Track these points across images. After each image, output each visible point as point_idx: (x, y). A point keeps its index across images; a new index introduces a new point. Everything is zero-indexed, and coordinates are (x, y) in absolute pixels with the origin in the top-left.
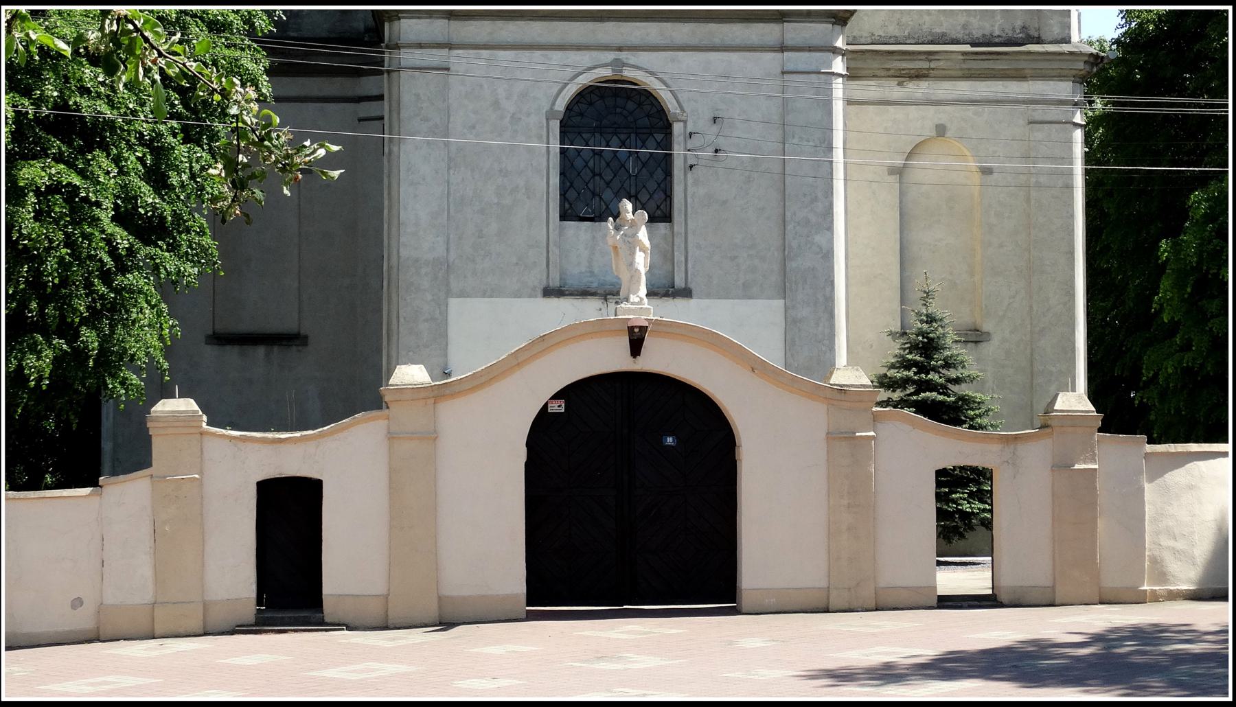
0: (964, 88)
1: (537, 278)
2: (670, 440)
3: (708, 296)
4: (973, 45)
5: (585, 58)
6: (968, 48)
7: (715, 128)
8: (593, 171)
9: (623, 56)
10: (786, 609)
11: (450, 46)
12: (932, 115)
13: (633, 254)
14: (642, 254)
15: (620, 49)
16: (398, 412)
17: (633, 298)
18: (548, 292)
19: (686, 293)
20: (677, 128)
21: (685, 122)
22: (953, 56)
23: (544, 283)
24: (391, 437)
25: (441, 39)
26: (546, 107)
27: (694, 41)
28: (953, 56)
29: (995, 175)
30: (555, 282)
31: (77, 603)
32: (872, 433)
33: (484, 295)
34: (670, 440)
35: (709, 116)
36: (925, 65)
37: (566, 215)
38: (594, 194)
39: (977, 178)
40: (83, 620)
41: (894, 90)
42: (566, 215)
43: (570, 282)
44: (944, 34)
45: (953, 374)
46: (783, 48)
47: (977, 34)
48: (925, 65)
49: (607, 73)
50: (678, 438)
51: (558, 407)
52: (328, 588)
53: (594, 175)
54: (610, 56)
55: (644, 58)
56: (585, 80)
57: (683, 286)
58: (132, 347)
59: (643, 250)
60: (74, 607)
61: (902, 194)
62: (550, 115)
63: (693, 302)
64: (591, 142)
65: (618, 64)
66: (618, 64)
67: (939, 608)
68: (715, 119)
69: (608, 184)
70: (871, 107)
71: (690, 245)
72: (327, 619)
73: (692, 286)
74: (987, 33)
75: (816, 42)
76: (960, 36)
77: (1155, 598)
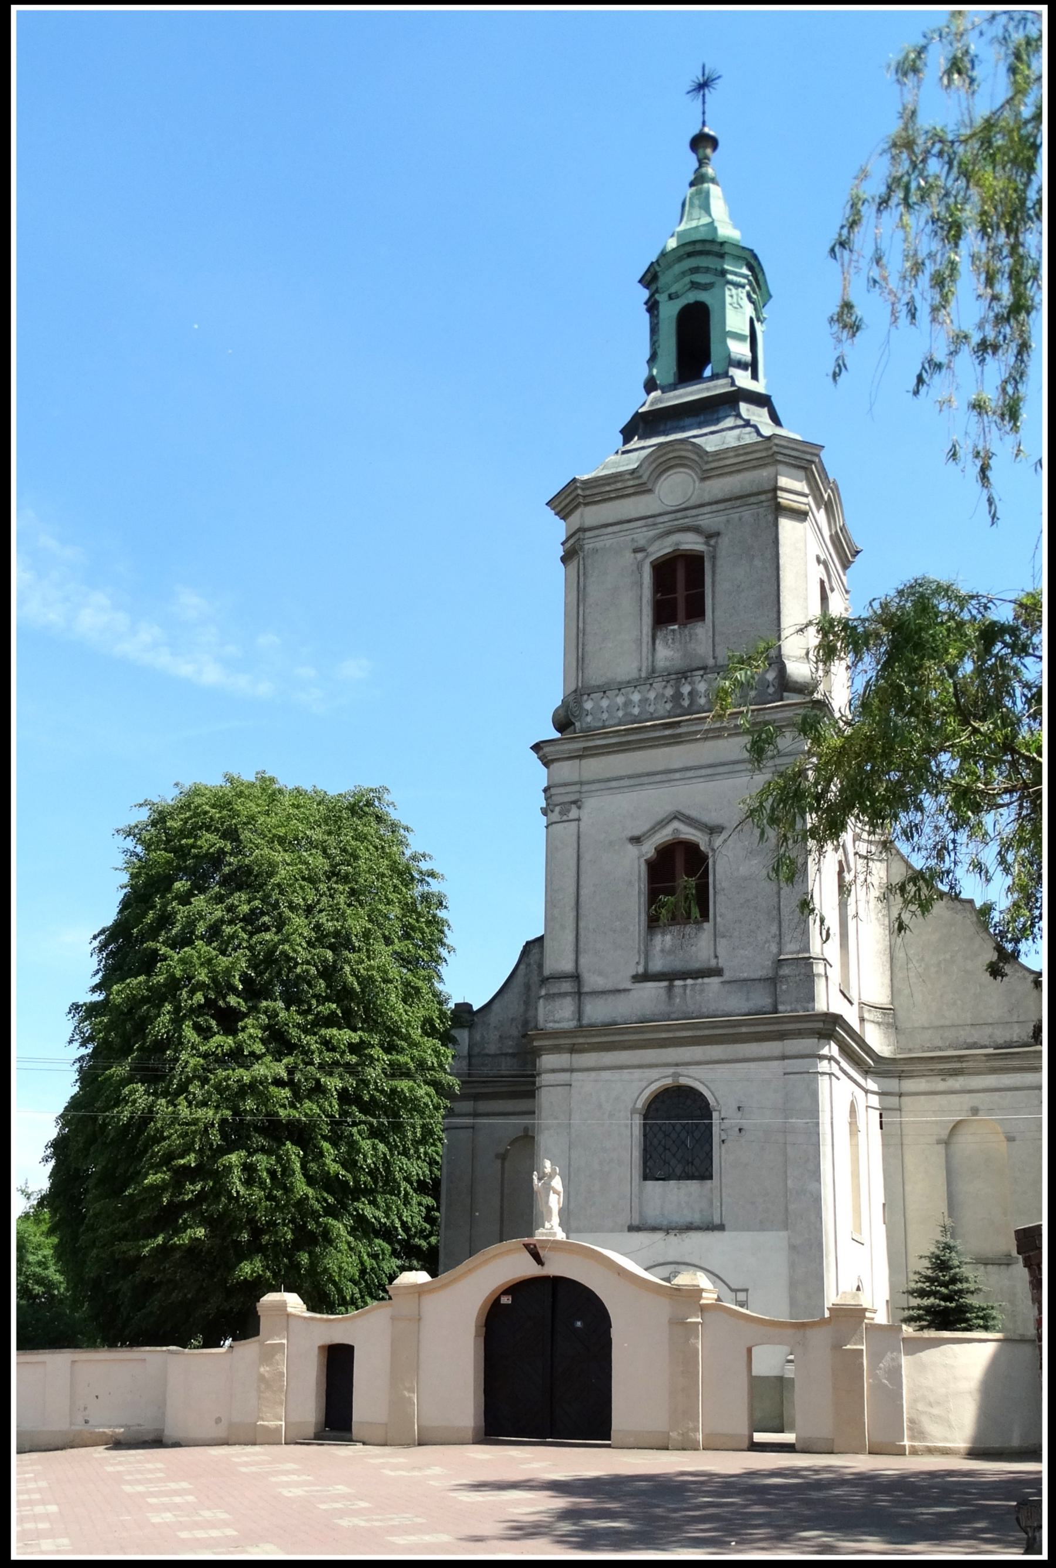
0: (991, 1081)
1: (624, 1220)
2: (579, 1324)
3: (736, 1229)
4: (995, 1048)
5: (654, 1073)
6: (991, 1051)
7: (740, 1114)
8: (665, 1147)
9: (680, 1070)
10: (640, 1445)
11: (572, 1070)
12: (967, 1100)
13: (548, 1196)
14: (556, 1196)
15: (677, 1065)
16: (400, 1304)
17: (547, 1225)
18: (632, 1229)
19: (721, 1228)
20: (715, 1115)
21: (720, 1111)
22: (978, 1058)
23: (628, 1223)
24: (393, 1318)
25: (566, 1066)
26: (630, 1106)
27: (723, 1057)
28: (978, 1058)
29: (1017, 1142)
30: (636, 1222)
31: (218, 1420)
32: (699, 1320)
33: (591, 1231)
34: (579, 1324)
35: (735, 1107)
36: (958, 1065)
37: (646, 1177)
38: (665, 1162)
39: (1005, 1144)
40: (220, 1432)
41: (940, 1085)
42: (646, 1177)
43: (649, 1222)
44: (975, 1043)
45: (959, 1286)
46: (784, 1058)
47: (1000, 1041)
48: (958, 1065)
49: (669, 1081)
50: (584, 1322)
51: (506, 1300)
52: (356, 1416)
53: (665, 1149)
54: (671, 1071)
55: (693, 1071)
56: (654, 1087)
57: (719, 1222)
58: (332, 1265)
59: (556, 1192)
60: (217, 1423)
61: (947, 1156)
62: (634, 1111)
63: (726, 1233)
64: (678, 1128)
65: (676, 1075)
66: (676, 1075)
67: (749, 1450)
68: (739, 1108)
69: (674, 1155)
70: (923, 1097)
71: (724, 1195)
72: (354, 1438)
73: (724, 1222)
74: (1008, 1040)
75: (808, 1052)
76: (987, 1043)
77: (914, 1452)
